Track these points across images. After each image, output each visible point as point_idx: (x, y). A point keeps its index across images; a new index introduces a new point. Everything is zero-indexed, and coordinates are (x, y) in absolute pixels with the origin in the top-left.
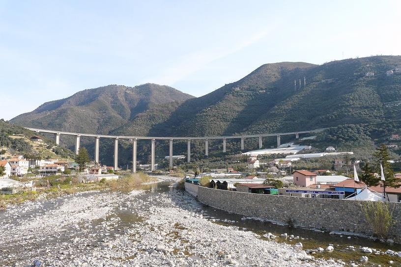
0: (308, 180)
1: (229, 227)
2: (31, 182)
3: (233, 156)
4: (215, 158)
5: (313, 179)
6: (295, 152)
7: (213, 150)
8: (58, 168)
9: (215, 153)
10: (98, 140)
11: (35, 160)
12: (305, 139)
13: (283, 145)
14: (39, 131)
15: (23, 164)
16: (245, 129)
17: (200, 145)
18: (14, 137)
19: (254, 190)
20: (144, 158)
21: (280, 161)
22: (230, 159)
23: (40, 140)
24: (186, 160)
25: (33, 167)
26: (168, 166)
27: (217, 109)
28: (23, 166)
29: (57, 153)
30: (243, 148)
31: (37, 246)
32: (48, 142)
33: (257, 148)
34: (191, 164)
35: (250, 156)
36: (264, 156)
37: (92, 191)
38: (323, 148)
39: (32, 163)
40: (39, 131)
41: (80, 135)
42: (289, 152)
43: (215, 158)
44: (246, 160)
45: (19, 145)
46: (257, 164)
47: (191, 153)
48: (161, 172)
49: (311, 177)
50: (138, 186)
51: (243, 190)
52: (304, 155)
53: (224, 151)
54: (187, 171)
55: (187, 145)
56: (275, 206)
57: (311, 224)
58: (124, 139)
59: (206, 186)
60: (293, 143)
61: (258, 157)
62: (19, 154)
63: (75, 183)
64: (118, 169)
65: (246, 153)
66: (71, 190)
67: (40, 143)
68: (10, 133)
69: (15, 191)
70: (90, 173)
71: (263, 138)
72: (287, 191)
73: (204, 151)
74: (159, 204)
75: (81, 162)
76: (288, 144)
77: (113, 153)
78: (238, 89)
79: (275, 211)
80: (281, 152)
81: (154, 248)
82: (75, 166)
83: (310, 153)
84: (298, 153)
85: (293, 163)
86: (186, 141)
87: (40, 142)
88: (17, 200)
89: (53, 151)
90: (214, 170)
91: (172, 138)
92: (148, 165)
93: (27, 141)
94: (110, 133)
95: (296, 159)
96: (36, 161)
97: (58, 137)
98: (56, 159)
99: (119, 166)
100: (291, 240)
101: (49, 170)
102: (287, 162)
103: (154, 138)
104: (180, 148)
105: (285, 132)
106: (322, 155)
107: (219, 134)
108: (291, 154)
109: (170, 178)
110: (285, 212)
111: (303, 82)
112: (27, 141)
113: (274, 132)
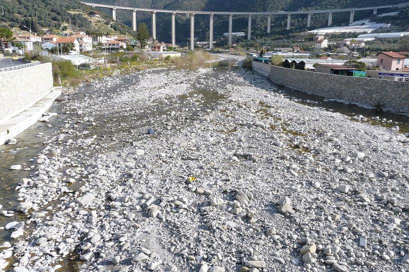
0: (394, 63)
1: (315, 108)
2: (103, 58)
3: (297, 34)
4: (277, 36)
5: (401, 62)
6: (370, 31)
7: (276, 26)
8: (120, 45)
9: (278, 30)
10: (154, 15)
11: (97, 37)
12: (384, 15)
13: (357, 22)
14: (94, 5)
15: (87, 41)
16: (313, 3)
18: (72, 12)
19: (336, 71)
20: (202, 35)
21: (352, 41)
22: (294, 37)
24: (246, 37)
25: (96, 43)
26: (227, 44)
28: (88, 42)
29: (115, 29)
30: (309, 26)
31: (141, 117)
32: (105, 17)
33: (325, 25)
34: (251, 42)
35: (316, 34)
36: (333, 35)
37: (159, 69)
38: (405, 27)
39: (94, 39)
40: (94, 5)
41: (136, 9)
42: (362, 31)
43: (277, 36)
44: (312, 38)
45: (79, 21)
46: (325, 44)
47: (252, 30)
48: (221, 50)
49: (399, 59)
50: (202, 64)
51: (324, 71)
52: (381, 34)
53: (288, 28)
54: (248, 49)
55: (248, 21)
56: (363, 89)
57: (402, 109)
58: (181, 14)
59: (279, 65)
60: (368, 21)
61: (326, 35)
62: (79, 30)
63: (142, 60)
64: (176, 46)
65: (312, 31)
66: (140, 66)
67: (98, 19)
68: (68, 8)
69: (92, 67)
70: (153, 50)
71: (334, 14)
72: (380, 74)
73: (266, 28)
74: (232, 82)
75: (142, 37)
76: (362, 22)
77: (171, 30)
79: (362, 94)
80: (352, 31)
81: (252, 123)
82: (135, 43)
83: (388, 32)
84: (373, 32)
85: (367, 43)
86: (246, 17)
87: (97, 17)
88: (97, 75)
89: (112, 27)
90: (278, 49)
91: (232, 13)
92: (206, 43)
93: (86, 16)
94: (165, 8)
95: (370, 39)
96: (98, 38)
97: (114, 12)
98: (115, 35)
99: (176, 44)
100: (384, 123)
101: (112, 47)
102: (360, 42)
103: (213, 13)
104: (240, 24)
105: (361, 7)
106: (402, 34)
107: (283, 9)
108: (365, 33)
109: (231, 57)
110: (374, 96)
112: (86, 16)
113: (347, 7)
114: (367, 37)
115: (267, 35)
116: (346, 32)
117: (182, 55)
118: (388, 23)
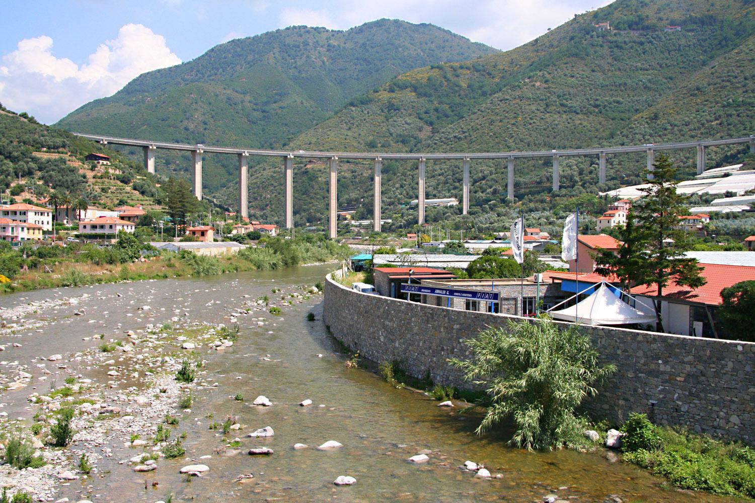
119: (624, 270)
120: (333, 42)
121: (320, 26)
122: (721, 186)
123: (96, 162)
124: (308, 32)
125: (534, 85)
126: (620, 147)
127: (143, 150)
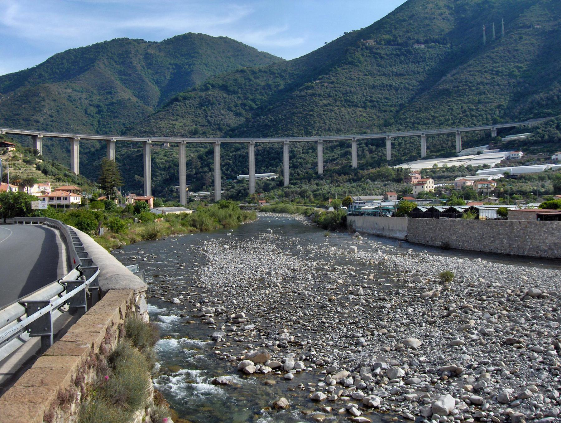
12: (509, 138)
13: (468, 150)
17: (303, 153)
23: (12, 149)
27: (332, 83)
29: (45, 172)
30: (389, 158)
42: (481, 163)
65: (400, 166)
73: (315, 165)
76: (476, 149)
78: (371, 42)
83: (523, 164)
86: (276, 146)
92: (208, 193)
111: (498, 31)
114: (489, 174)
115: (319, 177)
116: (454, 166)
117: (193, 212)
118: (519, 150)
119: (239, 240)
120: (150, 51)
121: (139, 39)
122: (475, 161)
123: (5, 148)
124: (130, 43)
125: (323, 85)
126: (398, 132)
127: (32, 138)
